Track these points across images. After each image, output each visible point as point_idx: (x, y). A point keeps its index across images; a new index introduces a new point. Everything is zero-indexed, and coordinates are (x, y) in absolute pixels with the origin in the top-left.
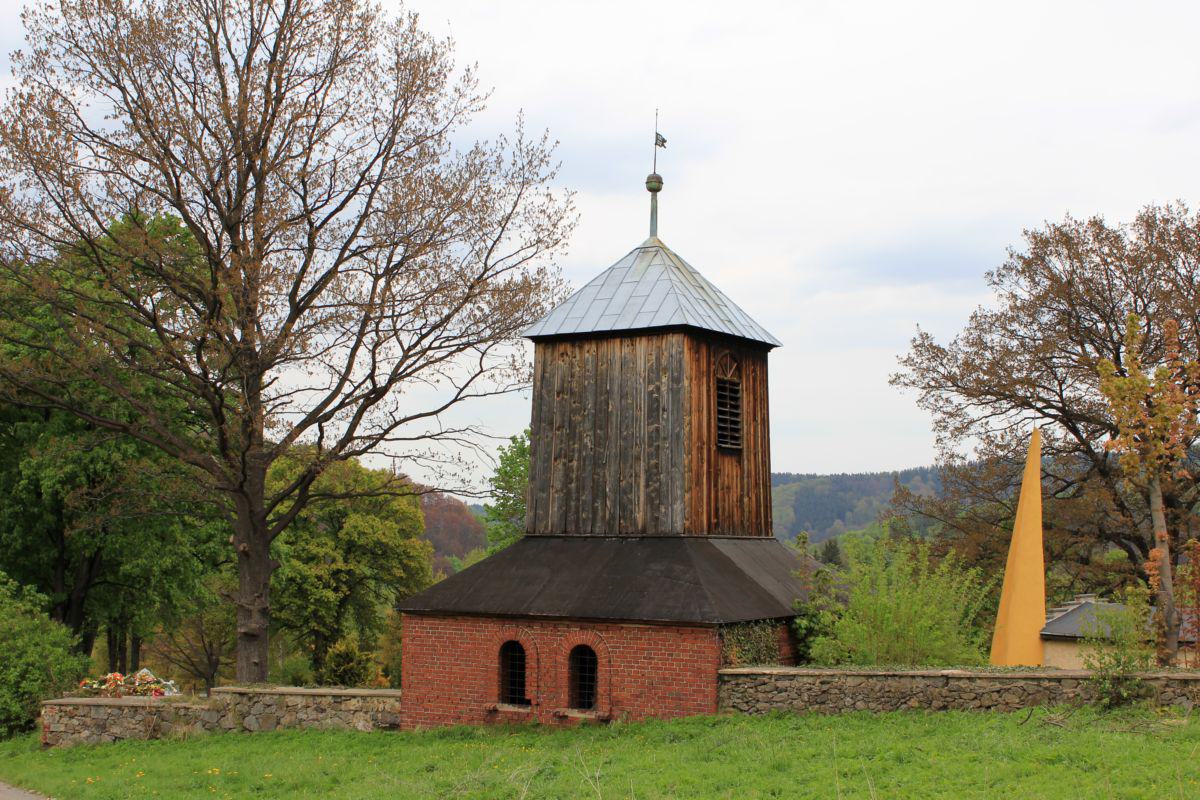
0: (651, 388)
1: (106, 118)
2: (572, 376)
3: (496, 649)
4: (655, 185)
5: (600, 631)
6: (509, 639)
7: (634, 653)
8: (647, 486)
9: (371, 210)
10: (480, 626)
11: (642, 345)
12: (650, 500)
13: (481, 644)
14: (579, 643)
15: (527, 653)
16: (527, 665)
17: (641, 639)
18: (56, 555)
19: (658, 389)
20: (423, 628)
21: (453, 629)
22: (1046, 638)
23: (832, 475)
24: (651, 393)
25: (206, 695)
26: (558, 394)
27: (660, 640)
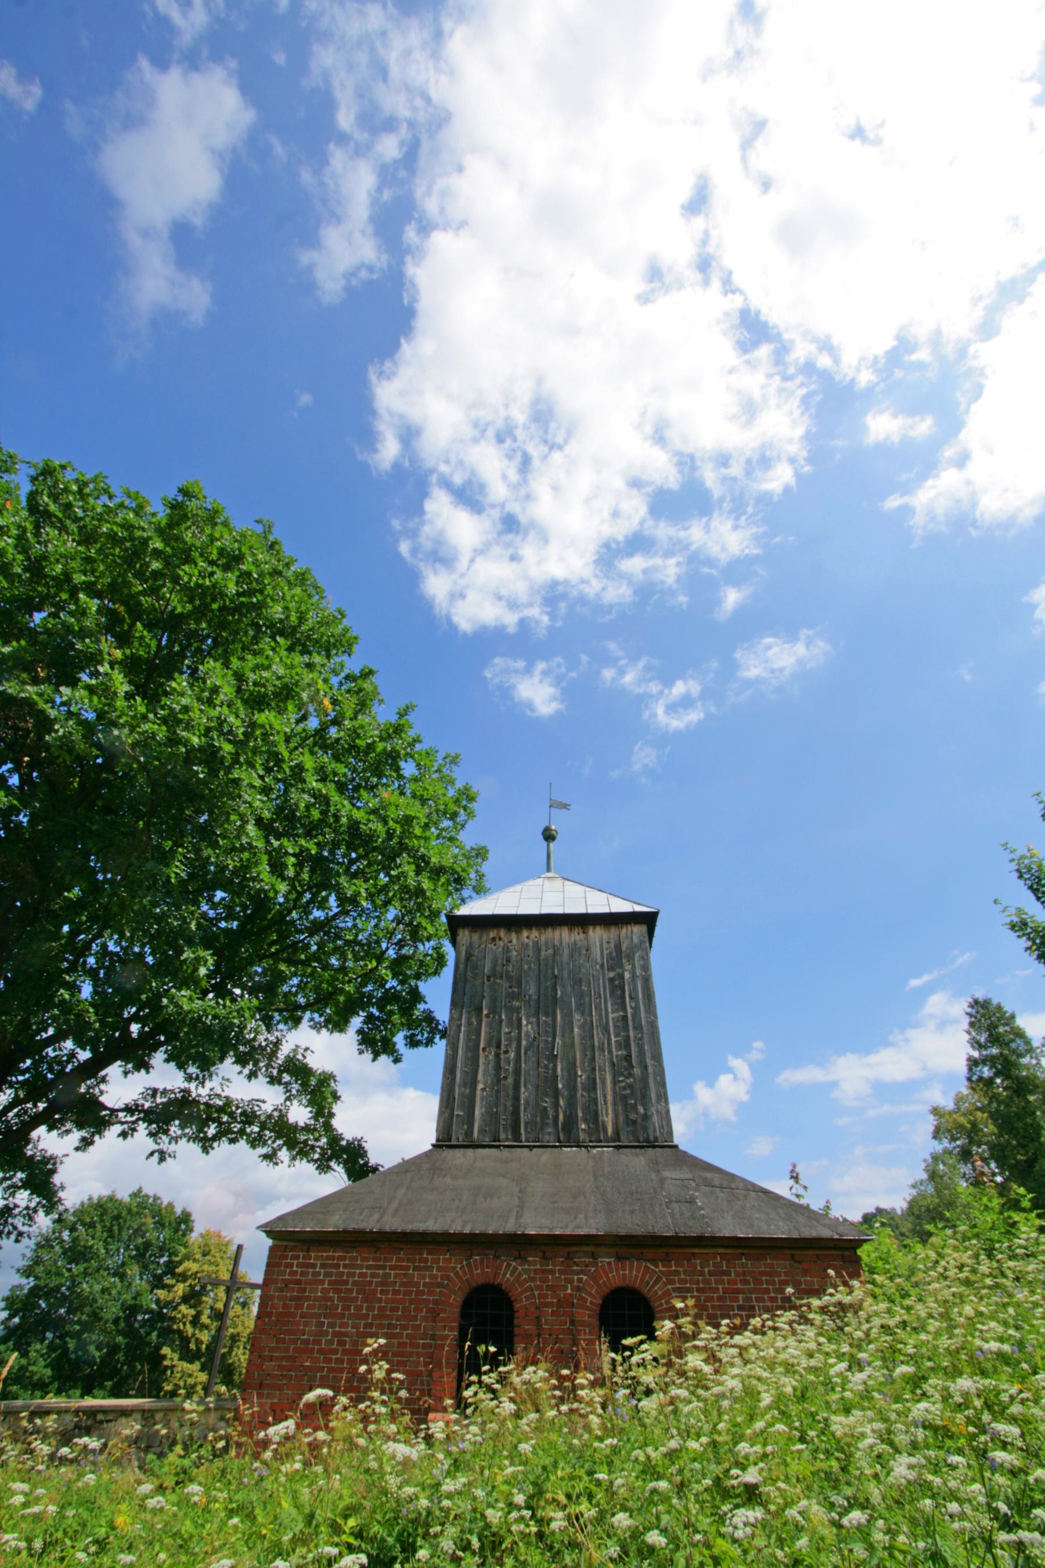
0: (612, 974)
1: (1005, 846)
2: (508, 961)
3: (456, 1300)
4: (549, 836)
5: (654, 1261)
6: (481, 1281)
7: (720, 1298)
8: (615, 1083)
9: (248, 1291)
10: (421, 1260)
11: (596, 934)
12: (621, 1099)
13: (423, 1293)
14: (617, 1283)
15: (517, 1306)
16: (516, 1331)
17: (728, 1273)
18: (114, 1070)
19: (621, 976)
20: (353, 1266)
21: (368, 1267)
22: (648, 920)
23: (878, 1052)
24: (611, 980)
25: (578, 609)
26: (489, 978)
27: (764, 1273)
